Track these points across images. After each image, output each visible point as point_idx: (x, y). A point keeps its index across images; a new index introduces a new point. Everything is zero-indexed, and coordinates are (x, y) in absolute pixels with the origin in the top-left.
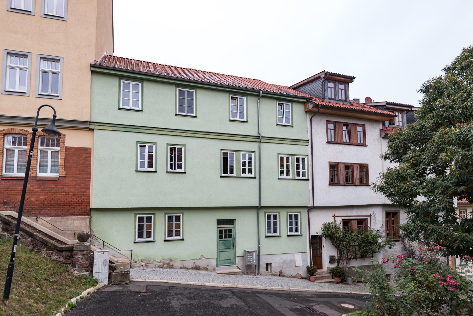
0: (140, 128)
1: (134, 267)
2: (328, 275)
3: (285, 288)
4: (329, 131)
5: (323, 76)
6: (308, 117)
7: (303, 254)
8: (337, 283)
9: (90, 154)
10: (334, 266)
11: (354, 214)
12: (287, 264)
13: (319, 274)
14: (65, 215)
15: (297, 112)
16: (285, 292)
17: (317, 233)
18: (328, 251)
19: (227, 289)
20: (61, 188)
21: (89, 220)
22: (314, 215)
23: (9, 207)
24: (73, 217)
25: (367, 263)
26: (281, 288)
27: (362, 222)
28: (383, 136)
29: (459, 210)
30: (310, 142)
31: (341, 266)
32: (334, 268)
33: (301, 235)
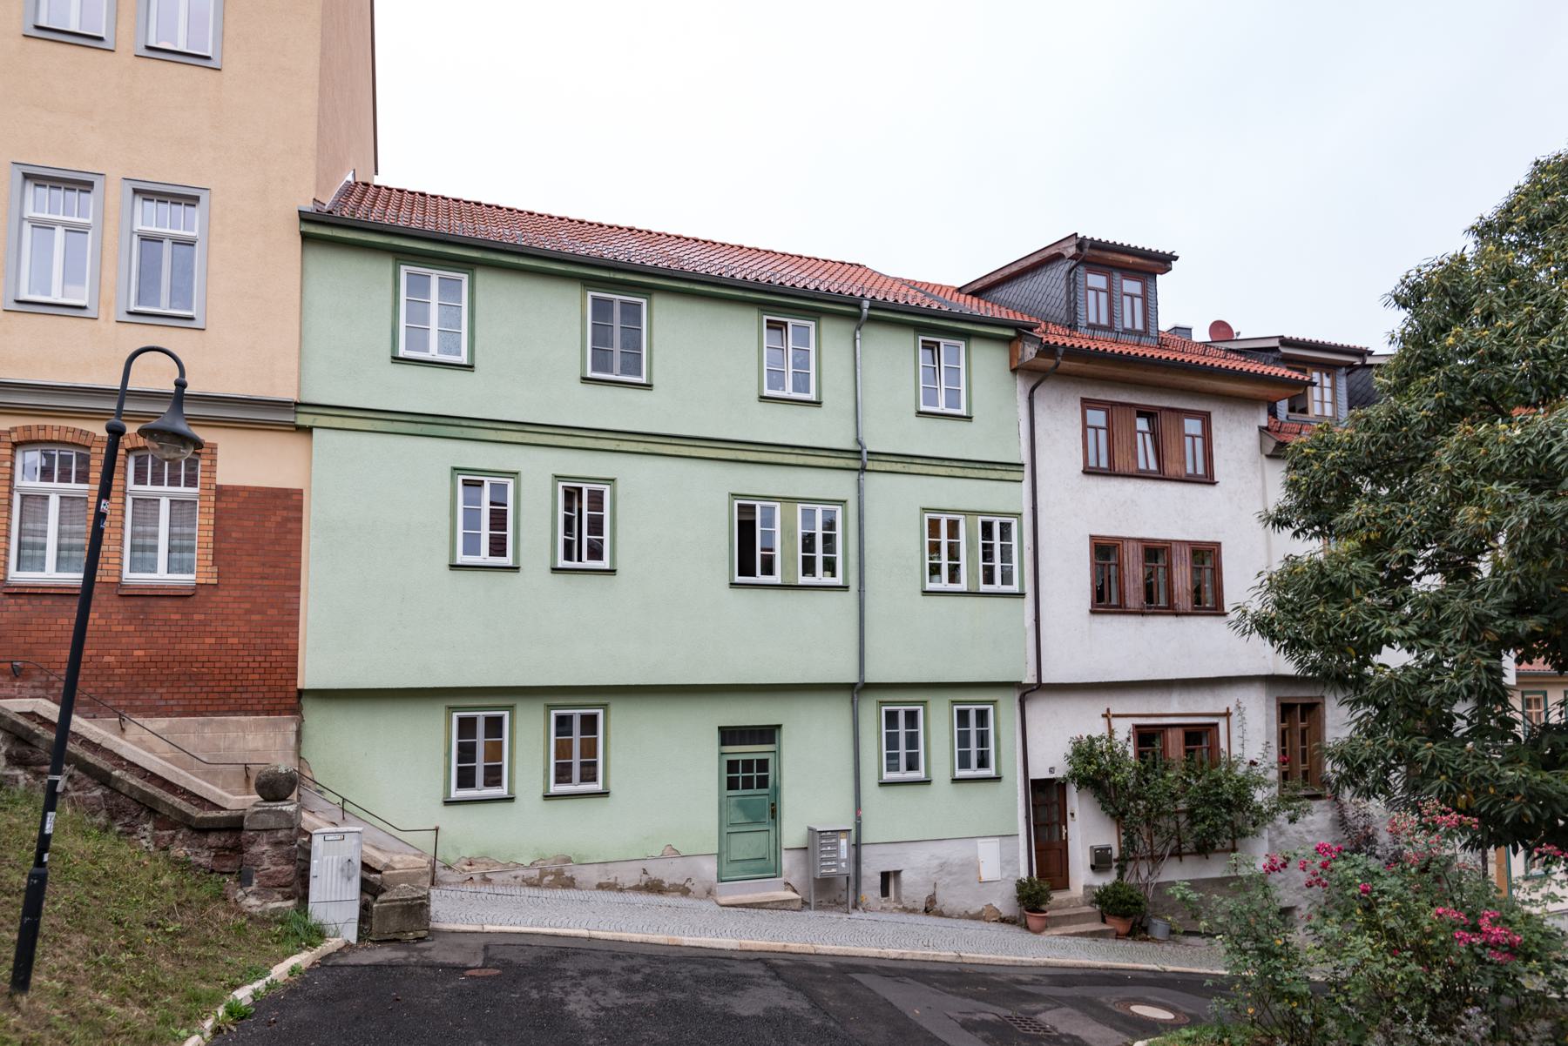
0: (464, 423)
1: (443, 883)
2: (1087, 909)
3: (946, 954)
4: (1091, 432)
5: (1072, 251)
6: (1021, 387)
7: (1006, 840)
8: (1118, 936)
9: (299, 509)
10: (1107, 879)
11: (1175, 708)
12: (950, 873)
13: (1058, 908)
14: (216, 713)
15: (984, 371)
16: (944, 968)
17: (1052, 770)
18: (1087, 830)
19: (754, 956)
20: (203, 623)
21: (294, 727)
22: (1040, 711)
23: (28, 684)
24: (243, 719)
25: (1215, 869)
26: (930, 953)
27: (1199, 736)
28: (1269, 451)
29: (1523, 693)
30: (1027, 469)
31: (1130, 879)
32: (1106, 888)
33: (998, 779)
